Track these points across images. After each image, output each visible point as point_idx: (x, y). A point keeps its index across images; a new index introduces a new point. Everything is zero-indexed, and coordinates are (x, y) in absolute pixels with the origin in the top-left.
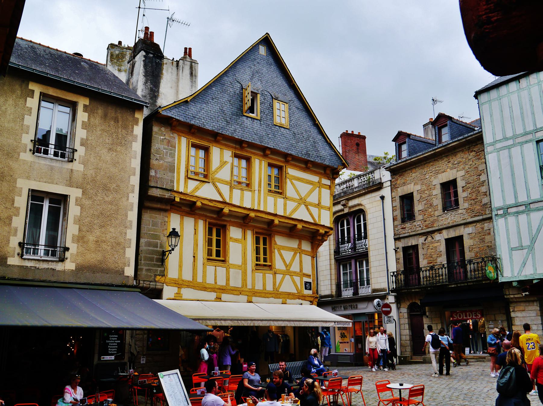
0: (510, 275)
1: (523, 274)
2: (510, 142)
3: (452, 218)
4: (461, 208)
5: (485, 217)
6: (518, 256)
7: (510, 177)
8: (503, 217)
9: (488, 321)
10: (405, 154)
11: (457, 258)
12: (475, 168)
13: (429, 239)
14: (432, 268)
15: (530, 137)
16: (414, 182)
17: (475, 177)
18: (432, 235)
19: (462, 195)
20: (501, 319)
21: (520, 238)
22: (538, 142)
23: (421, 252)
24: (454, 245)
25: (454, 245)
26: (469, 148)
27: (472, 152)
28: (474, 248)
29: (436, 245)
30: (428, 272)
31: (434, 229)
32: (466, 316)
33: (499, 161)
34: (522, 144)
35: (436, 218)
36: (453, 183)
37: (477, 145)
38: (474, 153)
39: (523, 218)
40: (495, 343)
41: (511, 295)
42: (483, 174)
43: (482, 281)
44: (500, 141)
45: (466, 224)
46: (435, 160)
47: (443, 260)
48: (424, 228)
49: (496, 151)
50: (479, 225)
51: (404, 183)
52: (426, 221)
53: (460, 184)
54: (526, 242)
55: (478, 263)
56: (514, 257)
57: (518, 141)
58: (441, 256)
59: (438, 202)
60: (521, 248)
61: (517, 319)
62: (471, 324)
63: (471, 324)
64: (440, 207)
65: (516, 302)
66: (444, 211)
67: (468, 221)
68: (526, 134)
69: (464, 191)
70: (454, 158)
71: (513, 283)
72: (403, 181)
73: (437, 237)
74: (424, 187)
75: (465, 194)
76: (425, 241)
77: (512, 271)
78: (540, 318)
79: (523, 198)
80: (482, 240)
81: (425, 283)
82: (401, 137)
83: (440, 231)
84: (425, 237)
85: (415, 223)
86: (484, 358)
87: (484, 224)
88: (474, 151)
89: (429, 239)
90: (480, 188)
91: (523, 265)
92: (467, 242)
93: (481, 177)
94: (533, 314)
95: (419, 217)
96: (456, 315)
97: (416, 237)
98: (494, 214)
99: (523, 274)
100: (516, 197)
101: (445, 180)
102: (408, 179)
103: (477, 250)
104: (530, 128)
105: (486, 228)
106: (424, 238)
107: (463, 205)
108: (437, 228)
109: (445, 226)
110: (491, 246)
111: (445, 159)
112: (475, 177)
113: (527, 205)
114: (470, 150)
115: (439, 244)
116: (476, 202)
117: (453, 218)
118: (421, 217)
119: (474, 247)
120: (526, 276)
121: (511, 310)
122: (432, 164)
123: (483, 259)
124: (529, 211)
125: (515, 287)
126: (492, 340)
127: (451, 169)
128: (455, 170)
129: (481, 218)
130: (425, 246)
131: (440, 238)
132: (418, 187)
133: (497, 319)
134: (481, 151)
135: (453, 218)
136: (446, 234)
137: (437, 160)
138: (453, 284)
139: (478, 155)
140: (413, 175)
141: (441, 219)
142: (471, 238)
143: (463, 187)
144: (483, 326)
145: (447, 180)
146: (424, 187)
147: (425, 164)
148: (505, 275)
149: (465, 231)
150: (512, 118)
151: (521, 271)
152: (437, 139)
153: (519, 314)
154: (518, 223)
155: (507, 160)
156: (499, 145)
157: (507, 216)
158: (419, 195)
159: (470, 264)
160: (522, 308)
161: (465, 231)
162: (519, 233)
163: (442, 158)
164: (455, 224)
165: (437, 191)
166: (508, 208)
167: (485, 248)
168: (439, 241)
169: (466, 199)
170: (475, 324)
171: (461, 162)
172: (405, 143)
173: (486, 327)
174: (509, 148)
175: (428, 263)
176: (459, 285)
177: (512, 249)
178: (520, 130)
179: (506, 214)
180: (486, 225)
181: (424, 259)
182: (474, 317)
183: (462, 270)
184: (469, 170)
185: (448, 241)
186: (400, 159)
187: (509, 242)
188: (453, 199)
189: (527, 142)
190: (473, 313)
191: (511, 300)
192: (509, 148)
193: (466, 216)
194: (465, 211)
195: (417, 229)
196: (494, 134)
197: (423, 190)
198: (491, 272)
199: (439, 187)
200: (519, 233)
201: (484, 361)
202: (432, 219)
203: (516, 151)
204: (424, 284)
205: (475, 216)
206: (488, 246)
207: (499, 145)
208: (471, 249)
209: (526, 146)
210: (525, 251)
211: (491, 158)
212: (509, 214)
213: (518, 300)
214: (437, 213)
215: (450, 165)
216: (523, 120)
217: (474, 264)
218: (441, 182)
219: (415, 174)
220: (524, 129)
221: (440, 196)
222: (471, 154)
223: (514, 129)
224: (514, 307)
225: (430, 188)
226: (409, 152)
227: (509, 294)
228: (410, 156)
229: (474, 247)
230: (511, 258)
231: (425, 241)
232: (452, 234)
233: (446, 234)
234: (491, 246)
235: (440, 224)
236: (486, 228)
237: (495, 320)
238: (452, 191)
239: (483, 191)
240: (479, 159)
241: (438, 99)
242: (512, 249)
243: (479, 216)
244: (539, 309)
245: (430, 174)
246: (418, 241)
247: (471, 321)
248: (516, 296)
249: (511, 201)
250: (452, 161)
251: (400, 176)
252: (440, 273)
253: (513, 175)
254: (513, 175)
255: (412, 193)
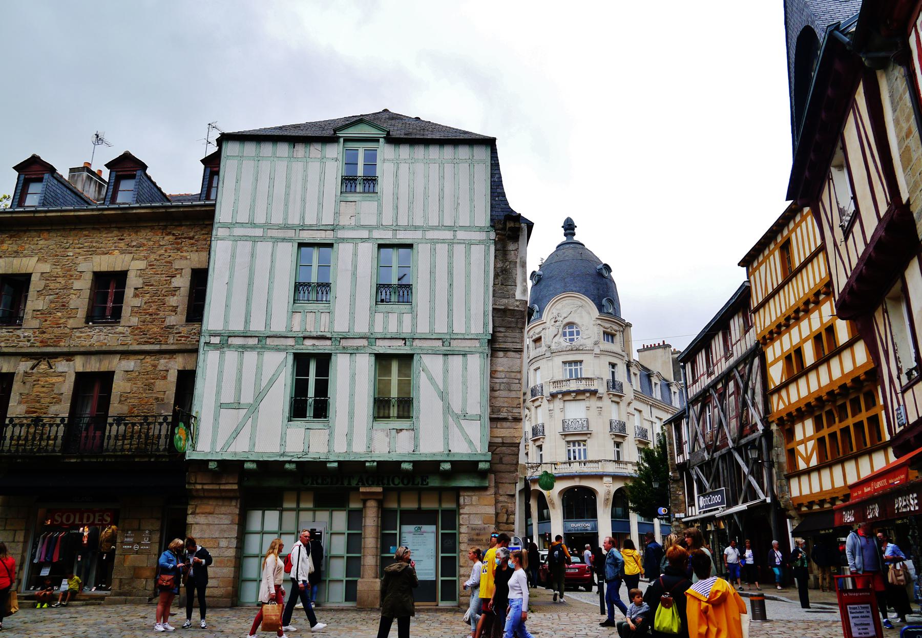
0: (208, 450)
1: (231, 449)
2: (258, 232)
3: (99, 337)
4: (122, 323)
5: (164, 347)
6: (229, 419)
7: (246, 286)
8: (217, 349)
9: (125, 531)
10: (32, 201)
11: (88, 411)
12: (167, 262)
13: (42, 367)
14: (37, 421)
15: (290, 234)
16: (40, 255)
17: (164, 278)
18: (51, 361)
19: (130, 300)
20: (150, 527)
21: (239, 390)
22: (301, 245)
23: (17, 387)
24: (92, 387)
25: (92, 387)
26: (165, 227)
27: (167, 235)
28: (131, 398)
29: (54, 380)
30: (24, 430)
31: (58, 350)
32: (81, 519)
33: (233, 256)
34: (276, 240)
35: (68, 331)
36: (120, 277)
37: (181, 226)
38: (170, 238)
39: (251, 357)
40: (175, 567)
41: (199, 484)
42: (178, 276)
43: (133, 456)
44: (242, 225)
45: (126, 354)
46: (94, 229)
47: (63, 409)
48: (38, 344)
49: (232, 238)
50: (149, 359)
51: (16, 252)
52: (44, 332)
53: (133, 281)
54: (247, 397)
55: (134, 424)
56: (221, 420)
57: (272, 232)
58: (59, 401)
59: (80, 302)
60: (237, 406)
61: (197, 527)
62: (85, 534)
63: (85, 534)
64: (82, 313)
65: (201, 498)
66: (87, 322)
67: (131, 348)
68: (286, 227)
69: (136, 296)
70: (134, 236)
71: (210, 463)
72: (15, 248)
73: (61, 366)
74: (59, 270)
75: (137, 302)
76: (32, 368)
77: (214, 442)
78: (236, 527)
79: (257, 325)
80: (150, 387)
81: (13, 449)
82: (35, 167)
83: (69, 356)
84: (35, 362)
85: (19, 332)
86: (102, 598)
87: (159, 359)
88: (174, 235)
89: (43, 366)
90: (167, 298)
91: (234, 435)
92: (119, 385)
93: (173, 280)
94: (226, 520)
95: (31, 322)
96: (61, 517)
97: (13, 359)
98: (203, 340)
99: (231, 449)
100: (247, 322)
101: (104, 268)
102: (27, 246)
103: (136, 402)
104: (295, 220)
105: (160, 367)
106: (30, 364)
107: (129, 318)
108: (66, 350)
109: (82, 349)
110: (163, 400)
111: (116, 233)
112: (164, 278)
113: (262, 338)
114: (165, 230)
115: (61, 379)
116: (154, 320)
117: (102, 338)
118: (35, 323)
119: (131, 395)
120: (235, 453)
121: (189, 512)
122: (86, 233)
123: (146, 418)
124: (262, 348)
125: (211, 470)
126: (169, 561)
127: (123, 252)
128: (128, 257)
129: (157, 347)
130: (30, 379)
131: (66, 369)
132: (46, 267)
133: (142, 528)
134: (185, 238)
135: (102, 338)
136: (79, 365)
137: (98, 229)
138: (74, 457)
139: (178, 243)
140: (41, 242)
141: (78, 334)
142: (129, 380)
143: (136, 289)
144: (112, 539)
145: (110, 270)
146: (59, 270)
147: (71, 230)
148: (199, 447)
149: (120, 366)
150: (270, 196)
151: (228, 444)
152: (110, 194)
153: (201, 519)
154: (241, 364)
155: (248, 259)
156: (238, 231)
157: (225, 349)
158: (43, 283)
159: (118, 425)
160: (208, 509)
161: (120, 366)
162: (239, 380)
163: (109, 229)
164: (104, 348)
165: (84, 284)
166: (229, 337)
167: (151, 401)
168: (62, 374)
169: (136, 311)
170: (94, 536)
171: (144, 245)
172: (40, 180)
173: (119, 541)
174: (254, 240)
175: (27, 412)
176: (86, 460)
177: (221, 406)
178: (277, 219)
179: (223, 346)
180: (162, 361)
181: (20, 403)
182: (96, 522)
183: (98, 433)
184: (155, 263)
185: (80, 376)
186: (20, 205)
187: (218, 393)
188: (110, 305)
189: (284, 240)
190: (97, 515)
191: (195, 494)
192: (254, 240)
193: (129, 340)
194: (129, 330)
195: (21, 344)
196: (235, 212)
197: (55, 274)
198: (180, 439)
199: (89, 277)
200: (239, 380)
201: (99, 604)
202: (57, 331)
203: (264, 248)
204: (9, 450)
205: (146, 343)
206: (157, 399)
207: (238, 231)
208: (123, 400)
209: (281, 245)
210: (243, 412)
211: (221, 249)
212: (229, 346)
213: (223, 494)
214: (71, 323)
215: (122, 245)
216: (286, 205)
217: (126, 425)
218: (96, 269)
219: (46, 242)
220: (286, 219)
221: (86, 294)
222: (167, 238)
223: (268, 214)
224: (196, 506)
225: (70, 273)
226: (45, 198)
227: (196, 483)
228: (44, 205)
229: (131, 395)
230: (216, 419)
231: (32, 368)
232: (94, 365)
233: (79, 365)
234: (163, 400)
235: (73, 343)
236: (160, 367)
237: (139, 529)
238: (112, 290)
239: (171, 304)
240: (178, 250)
241: (106, 138)
242: (221, 406)
243: (153, 343)
244: (237, 511)
245: (78, 251)
246: (16, 366)
247: (86, 529)
248: (206, 487)
249: (237, 325)
250: (128, 239)
251: (11, 237)
252: (52, 435)
253: (250, 284)
254: (250, 284)
255: (30, 275)
